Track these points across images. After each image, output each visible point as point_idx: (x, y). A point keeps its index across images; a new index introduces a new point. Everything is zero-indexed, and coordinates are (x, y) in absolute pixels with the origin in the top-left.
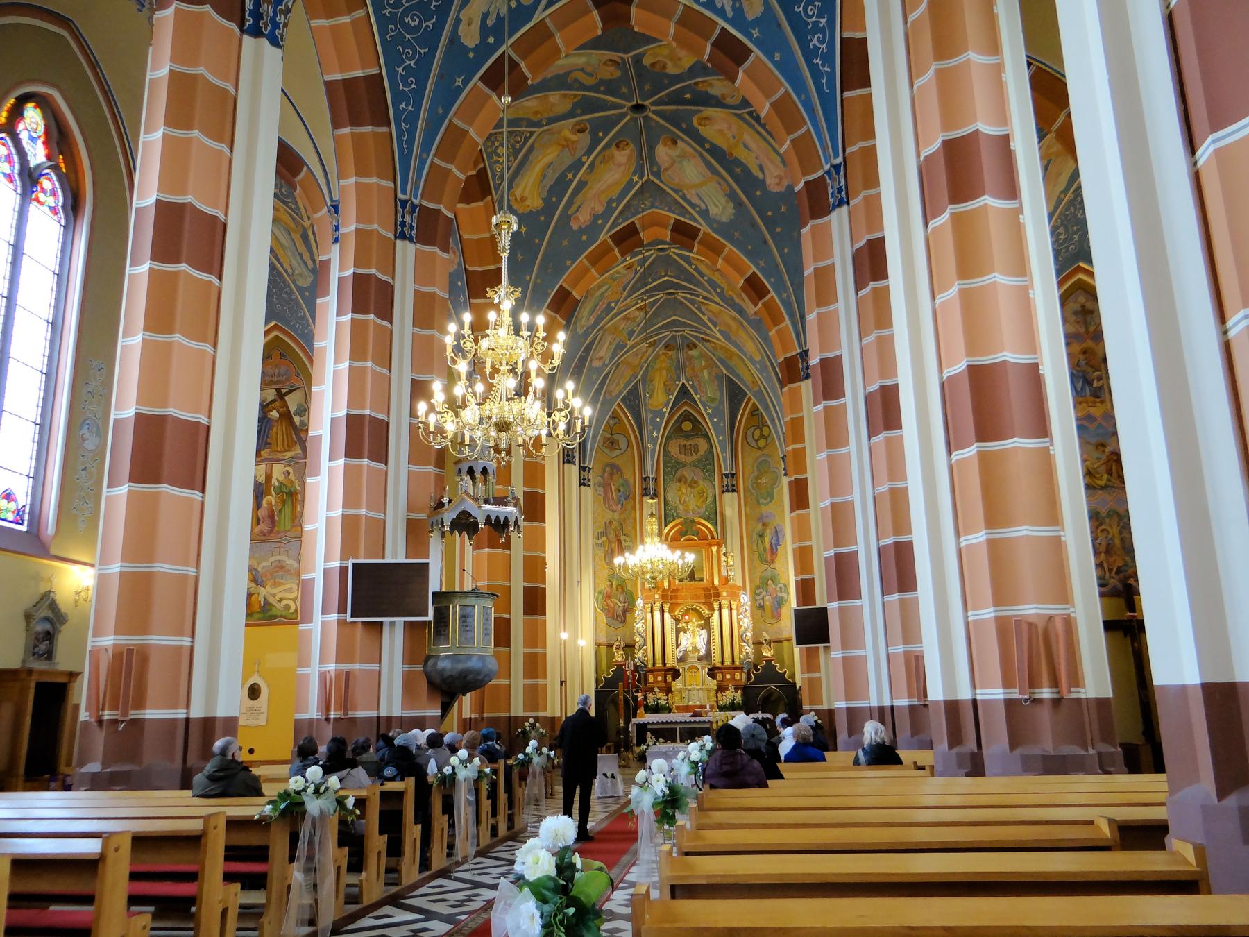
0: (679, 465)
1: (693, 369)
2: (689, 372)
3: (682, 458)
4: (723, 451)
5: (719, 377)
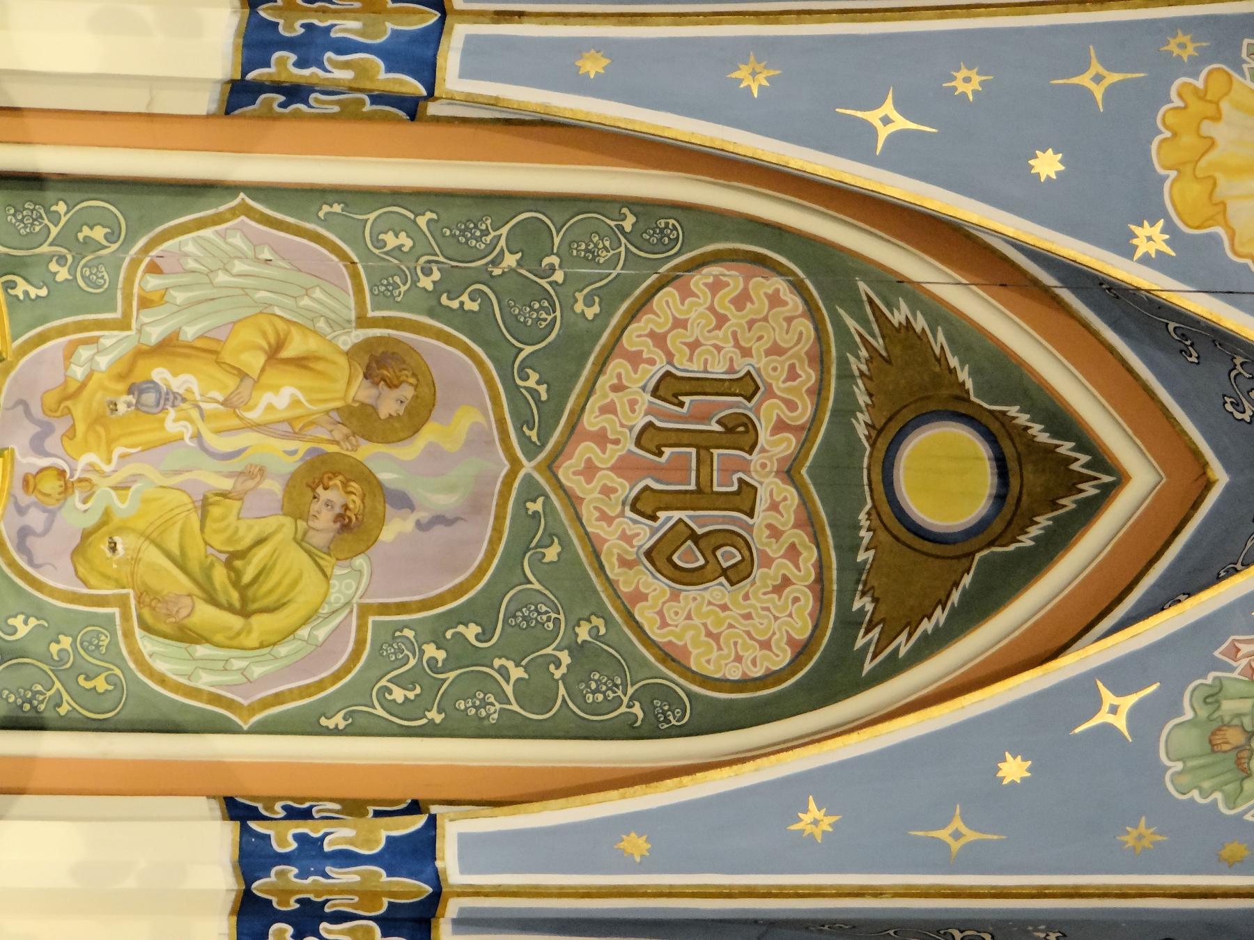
0: (546, 379)
3: (620, 403)
4: (674, 835)
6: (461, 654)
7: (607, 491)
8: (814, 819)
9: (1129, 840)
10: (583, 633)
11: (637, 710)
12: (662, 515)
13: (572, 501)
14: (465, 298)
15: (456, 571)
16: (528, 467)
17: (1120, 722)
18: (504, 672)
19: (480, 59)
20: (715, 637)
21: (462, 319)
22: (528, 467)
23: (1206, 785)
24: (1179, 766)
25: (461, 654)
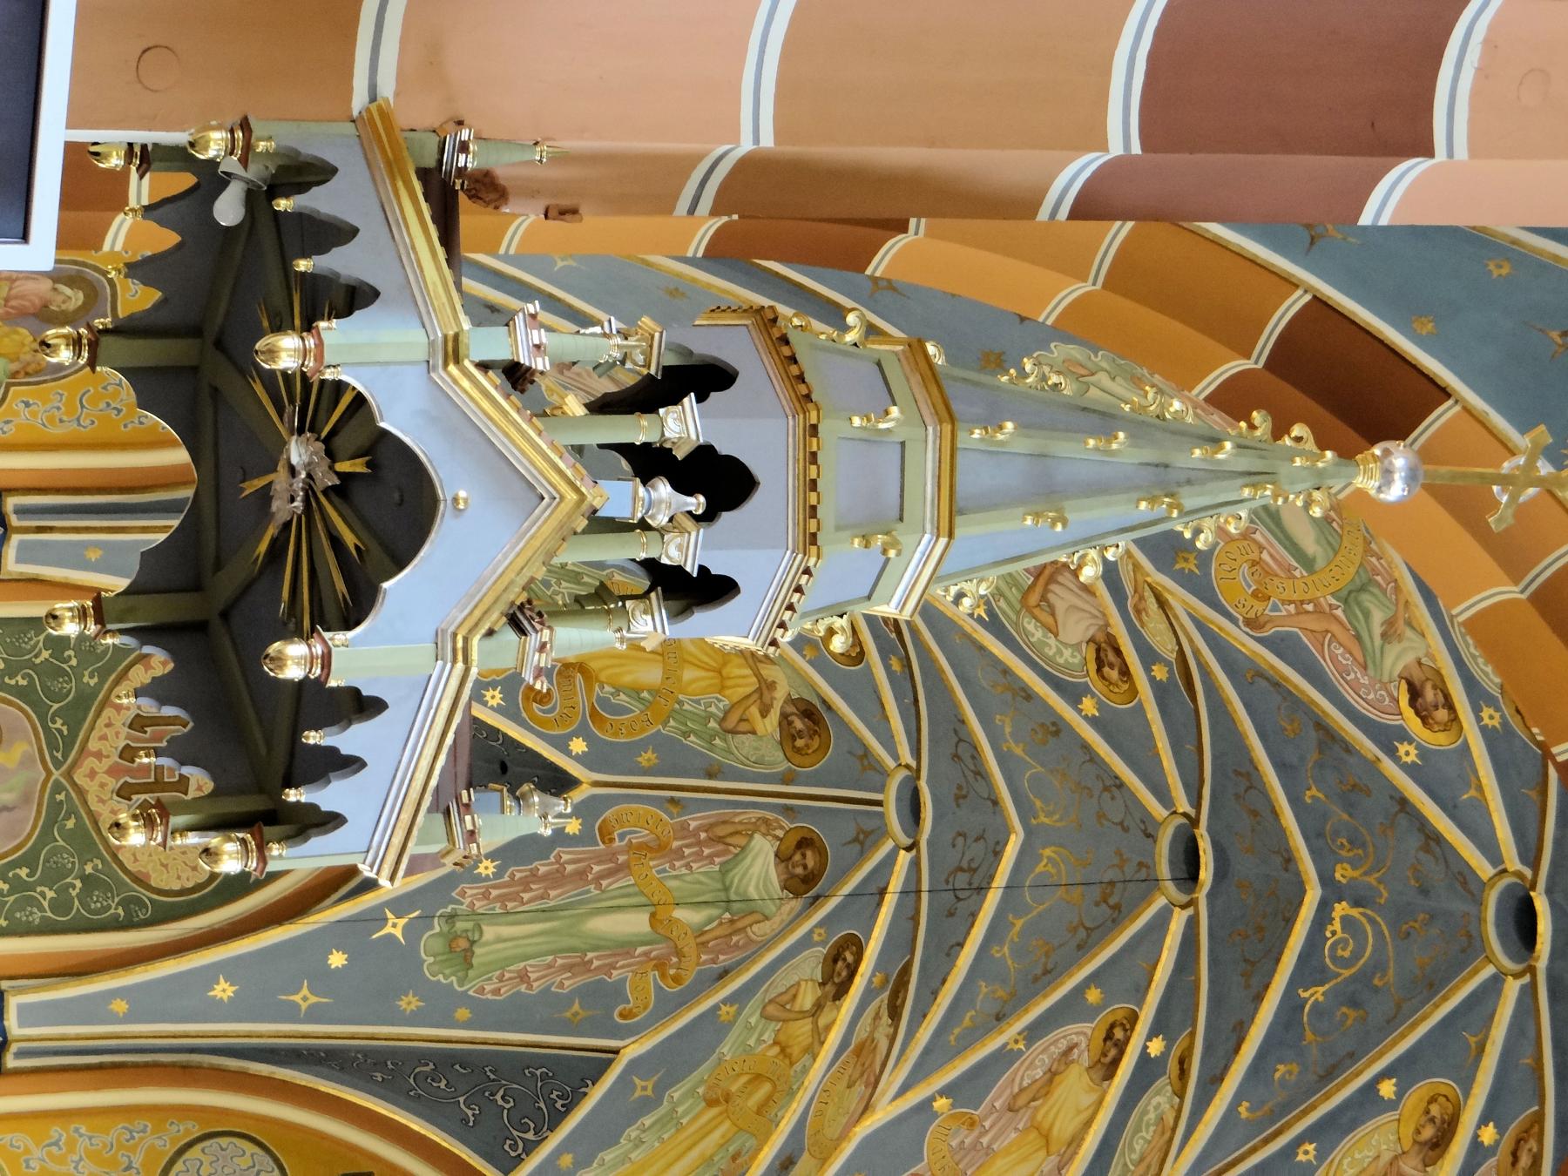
1: (658, 848)
2: (638, 821)
4: (144, 1003)
5: (602, 1001)
6: (17, 885)
7: (102, 785)
8: (223, 990)
9: (403, 1004)
10: (89, 869)
11: (120, 911)
12: (134, 797)
13: (81, 792)
14: (19, 678)
15: (16, 837)
16: (56, 774)
17: (398, 933)
18: (43, 894)
19: (25, 555)
20: (166, 866)
21: (19, 692)
22: (56, 774)
23: (447, 972)
24: (431, 959)
25: (17, 885)
